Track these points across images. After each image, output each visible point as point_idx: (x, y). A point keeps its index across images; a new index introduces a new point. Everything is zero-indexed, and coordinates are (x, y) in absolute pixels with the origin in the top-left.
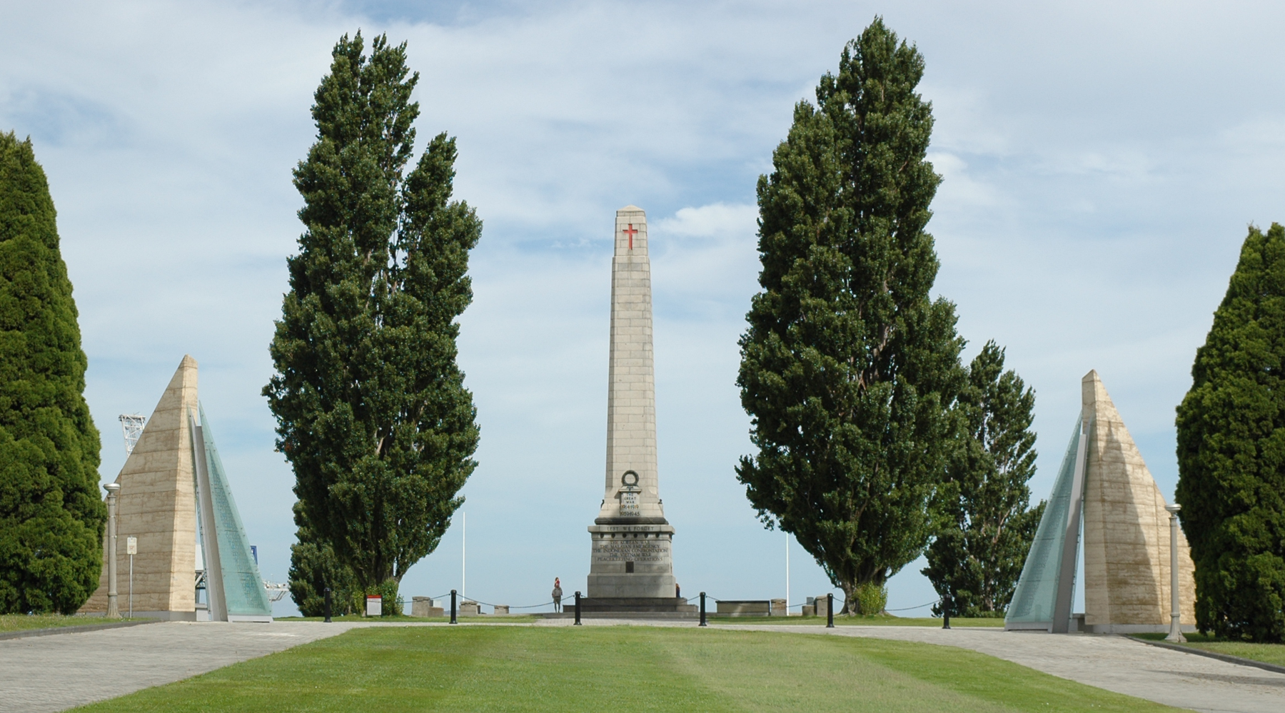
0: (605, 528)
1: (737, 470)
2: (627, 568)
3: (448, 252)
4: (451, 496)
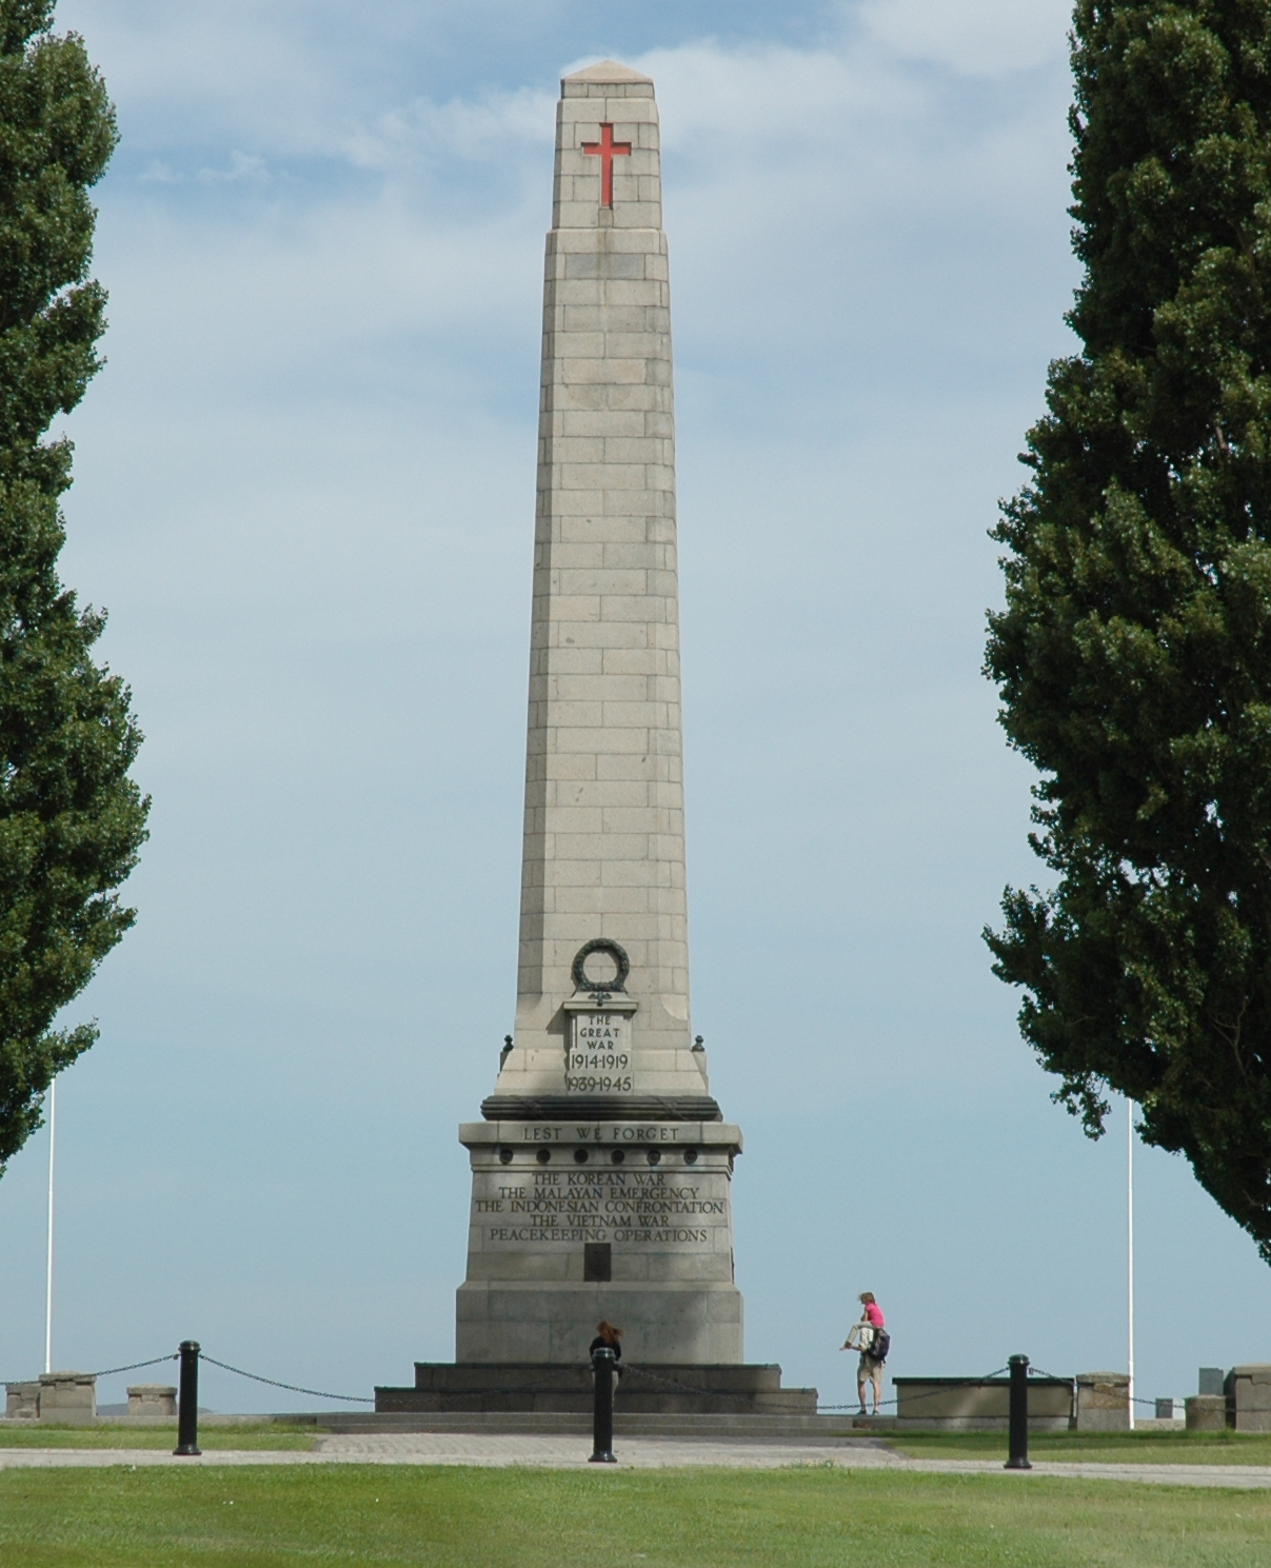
0: (509, 1131)
1: (995, 945)
2: (588, 1265)
3: (28, 209)
4: (42, 1021)
